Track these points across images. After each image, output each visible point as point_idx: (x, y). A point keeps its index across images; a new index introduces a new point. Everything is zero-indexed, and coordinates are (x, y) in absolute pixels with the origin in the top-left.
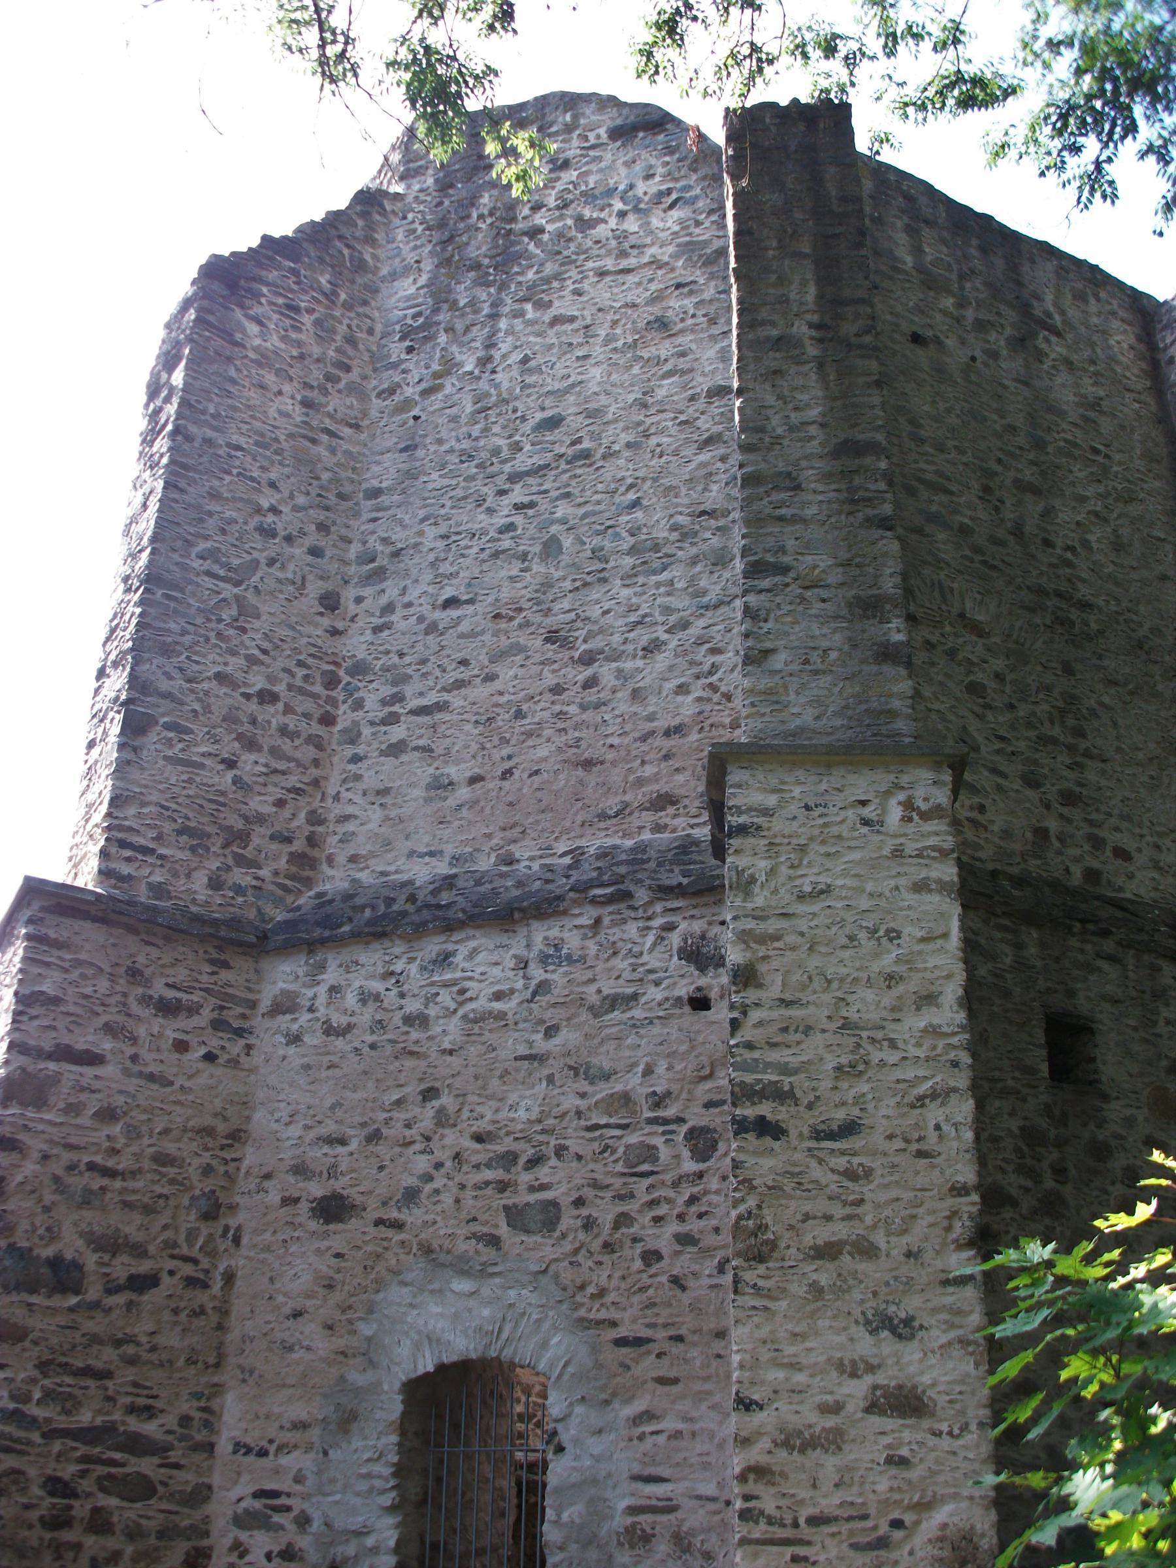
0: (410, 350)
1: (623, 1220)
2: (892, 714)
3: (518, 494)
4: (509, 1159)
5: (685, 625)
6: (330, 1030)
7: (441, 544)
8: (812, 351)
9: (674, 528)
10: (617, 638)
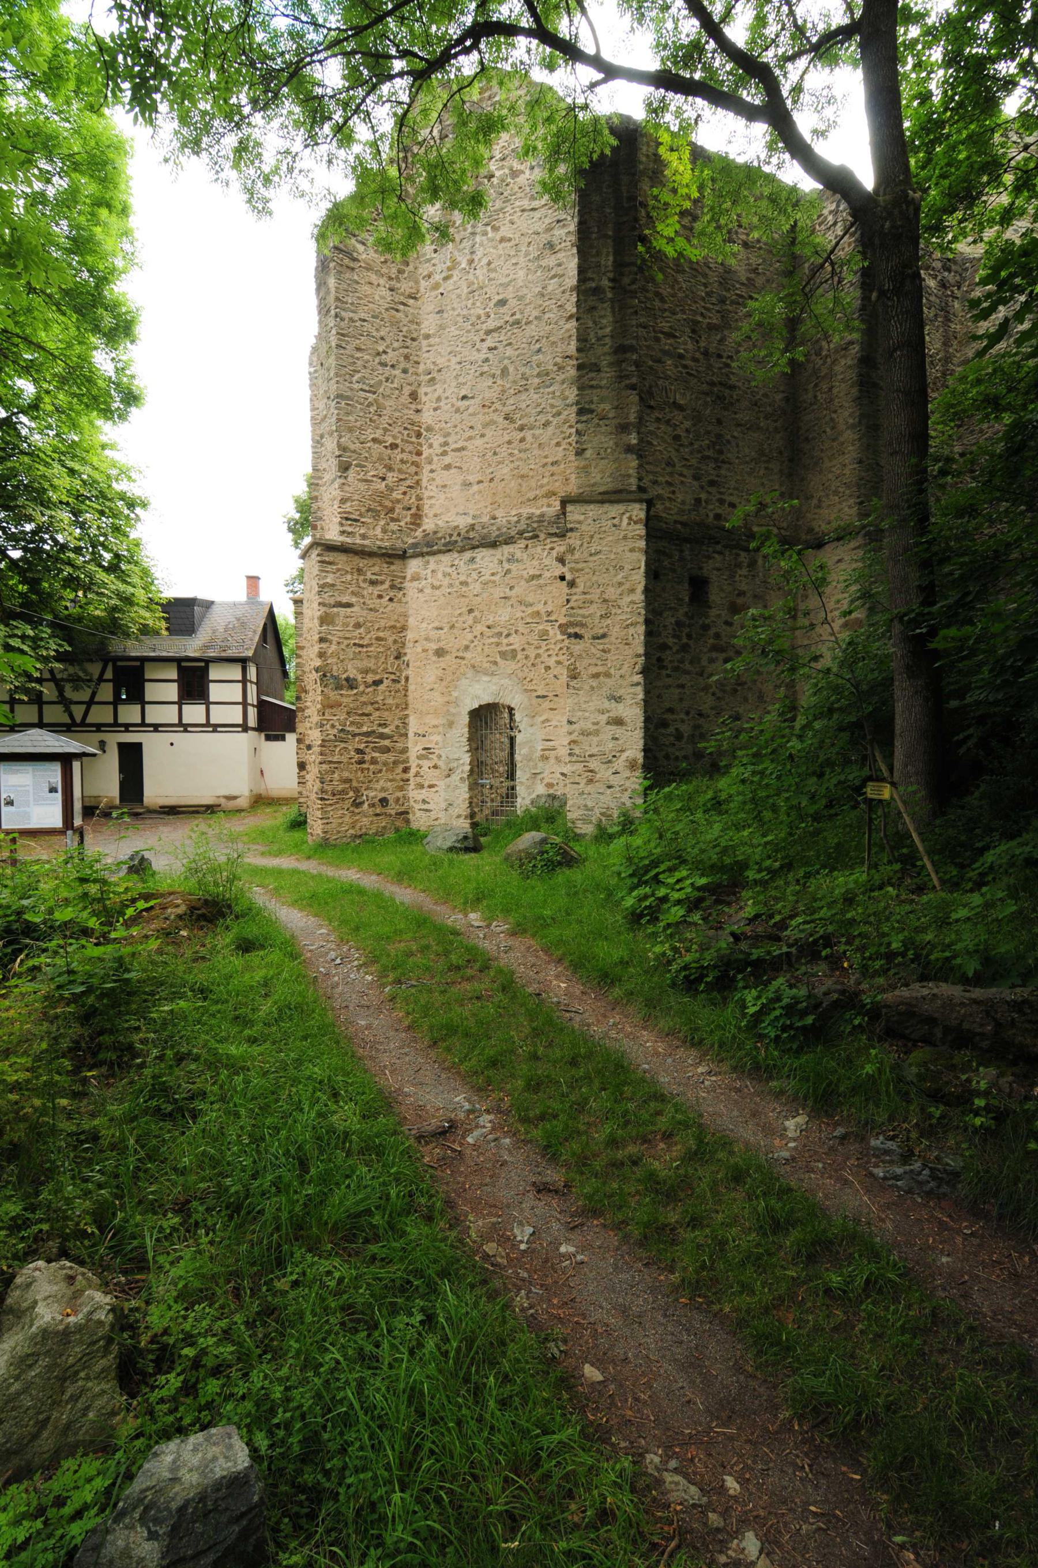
0: (435, 251)
1: (538, 656)
2: (629, 476)
3: (490, 342)
4: (500, 634)
5: (559, 414)
6: (433, 587)
7: (458, 367)
8: (610, 295)
9: (555, 365)
10: (532, 419)
